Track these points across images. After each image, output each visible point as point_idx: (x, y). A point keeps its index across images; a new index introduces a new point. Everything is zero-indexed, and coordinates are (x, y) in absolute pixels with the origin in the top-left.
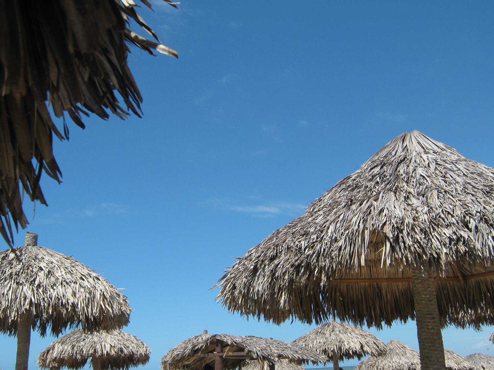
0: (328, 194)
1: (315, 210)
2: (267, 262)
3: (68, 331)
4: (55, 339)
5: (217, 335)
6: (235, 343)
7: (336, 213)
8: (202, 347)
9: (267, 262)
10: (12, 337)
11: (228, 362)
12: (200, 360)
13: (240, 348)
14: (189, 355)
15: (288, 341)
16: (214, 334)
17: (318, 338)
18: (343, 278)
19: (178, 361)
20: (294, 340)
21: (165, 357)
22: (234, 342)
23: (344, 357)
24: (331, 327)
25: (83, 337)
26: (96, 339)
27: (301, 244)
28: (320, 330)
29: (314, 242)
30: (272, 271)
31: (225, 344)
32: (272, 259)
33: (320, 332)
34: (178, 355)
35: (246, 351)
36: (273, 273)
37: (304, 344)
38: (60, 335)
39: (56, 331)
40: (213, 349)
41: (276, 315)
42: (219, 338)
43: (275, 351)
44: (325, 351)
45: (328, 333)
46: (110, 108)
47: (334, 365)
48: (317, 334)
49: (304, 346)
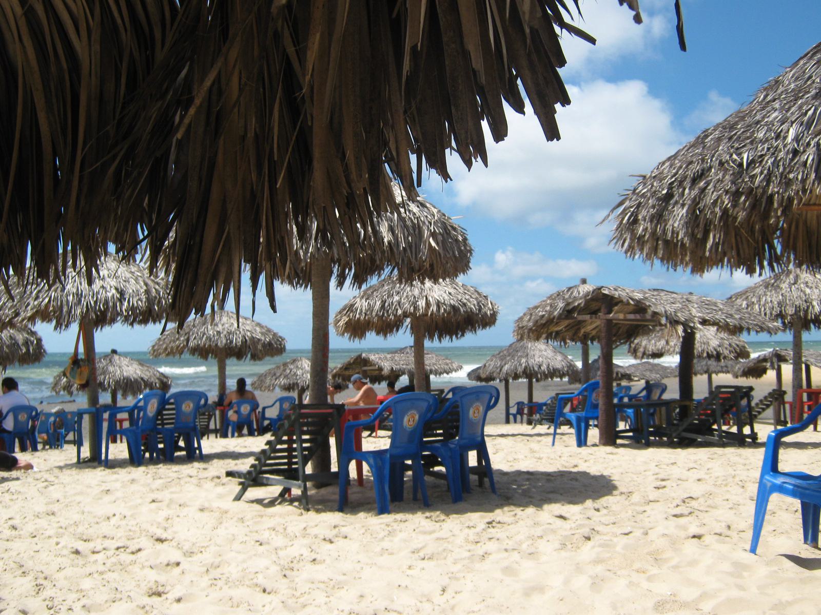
0: (791, 71)
1: (769, 98)
2: (687, 184)
3: (374, 281)
4: (356, 292)
5: (603, 287)
6: (632, 299)
7: (800, 107)
8: (579, 304)
9: (687, 184)
10: (300, 290)
11: (619, 328)
12: (577, 325)
13: (640, 308)
14: (560, 317)
15: (718, 298)
16: (600, 285)
17: (769, 293)
18: (812, 202)
19: (543, 325)
20: (729, 296)
21: (521, 319)
22: (218, 79)
23: (812, 326)
24: (791, 277)
25: (397, 289)
26: (416, 292)
27: (743, 158)
28: (773, 281)
29: (762, 156)
30: (695, 197)
31: (616, 301)
32: (694, 181)
33: (773, 284)
34: (543, 316)
35: (650, 312)
36: (695, 202)
37: (745, 303)
38: (364, 287)
39: (359, 280)
40: (597, 308)
41: (700, 265)
42: (606, 292)
43: (696, 313)
44: (781, 315)
45: (784, 286)
46: (766, 452)
47: (795, 337)
48: (766, 287)
49: (744, 305)
